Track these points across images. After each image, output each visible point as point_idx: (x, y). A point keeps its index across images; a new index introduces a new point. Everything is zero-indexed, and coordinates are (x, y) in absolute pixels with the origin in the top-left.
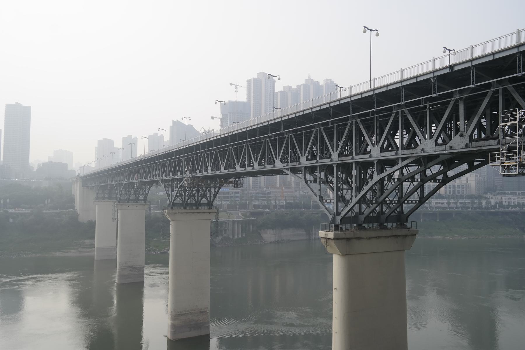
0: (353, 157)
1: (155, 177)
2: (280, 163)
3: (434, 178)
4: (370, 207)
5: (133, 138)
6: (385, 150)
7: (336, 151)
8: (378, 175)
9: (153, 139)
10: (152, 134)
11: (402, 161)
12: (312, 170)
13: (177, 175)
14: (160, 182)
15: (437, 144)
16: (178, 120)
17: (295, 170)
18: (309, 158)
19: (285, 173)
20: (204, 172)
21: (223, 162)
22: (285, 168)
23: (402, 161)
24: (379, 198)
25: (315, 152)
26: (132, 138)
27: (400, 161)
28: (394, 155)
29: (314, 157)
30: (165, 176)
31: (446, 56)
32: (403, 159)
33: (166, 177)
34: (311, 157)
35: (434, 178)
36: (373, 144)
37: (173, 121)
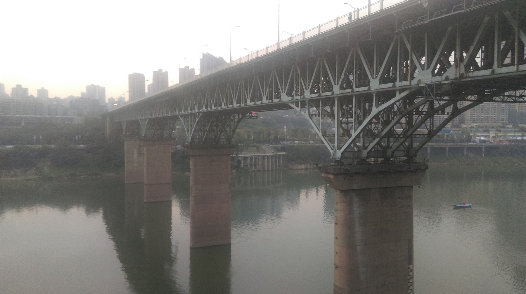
0: (494, 70)
1: (175, 112)
2: (286, 97)
3: (442, 109)
4: (399, 140)
5: (164, 72)
6: (436, 75)
7: (338, 84)
8: (376, 108)
9: (185, 72)
10: (183, 68)
11: (400, 94)
12: (315, 102)
13: (260, 101)
14: (180, 117)
15: (433, 74)
16: (208, 52)
17: (303, 104)
18: (344, 86)
19: (291, 107)
20: (219, 107)
21: (284, 91)
22: (290, 102)
23: (400, 94)
24: (382, 132)
25: (351, 81)
26: (163, 72)
27: (398, 93)
28: (350, 92)
29: (350, 86)
30: (215, 107)
31: (378, 2)
32: (402, 90)
33: (191, 111)
34: (347, 85)
35: (442, 109)
36: (422, 67)
37: (203, 53)
